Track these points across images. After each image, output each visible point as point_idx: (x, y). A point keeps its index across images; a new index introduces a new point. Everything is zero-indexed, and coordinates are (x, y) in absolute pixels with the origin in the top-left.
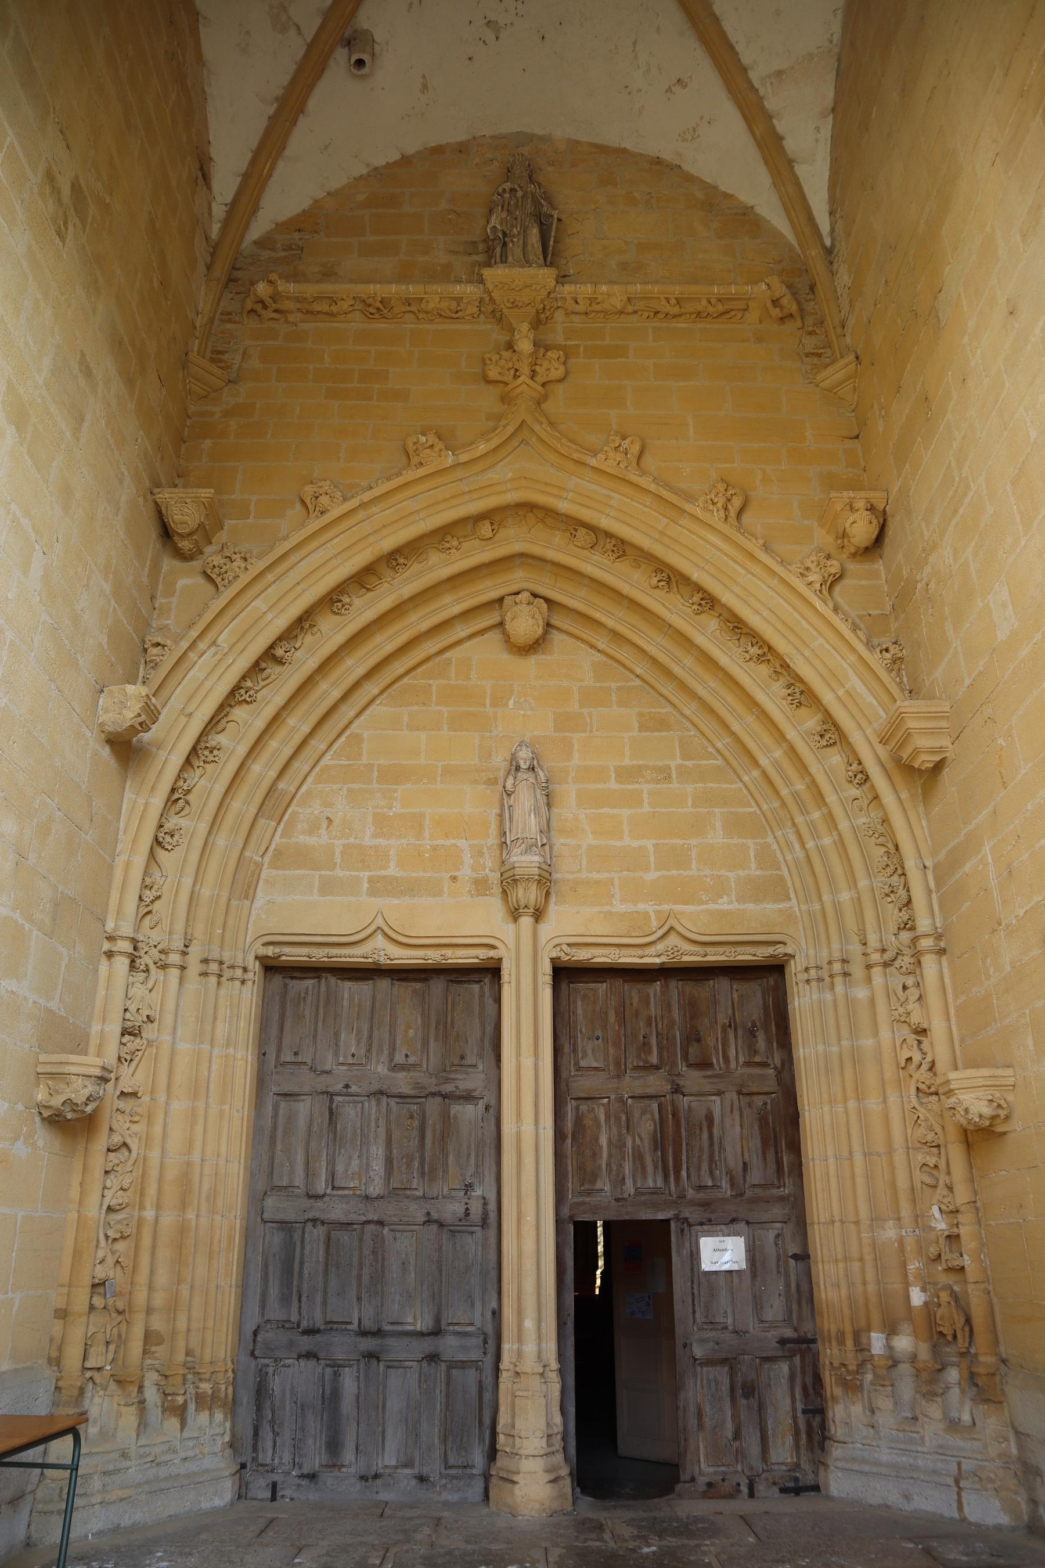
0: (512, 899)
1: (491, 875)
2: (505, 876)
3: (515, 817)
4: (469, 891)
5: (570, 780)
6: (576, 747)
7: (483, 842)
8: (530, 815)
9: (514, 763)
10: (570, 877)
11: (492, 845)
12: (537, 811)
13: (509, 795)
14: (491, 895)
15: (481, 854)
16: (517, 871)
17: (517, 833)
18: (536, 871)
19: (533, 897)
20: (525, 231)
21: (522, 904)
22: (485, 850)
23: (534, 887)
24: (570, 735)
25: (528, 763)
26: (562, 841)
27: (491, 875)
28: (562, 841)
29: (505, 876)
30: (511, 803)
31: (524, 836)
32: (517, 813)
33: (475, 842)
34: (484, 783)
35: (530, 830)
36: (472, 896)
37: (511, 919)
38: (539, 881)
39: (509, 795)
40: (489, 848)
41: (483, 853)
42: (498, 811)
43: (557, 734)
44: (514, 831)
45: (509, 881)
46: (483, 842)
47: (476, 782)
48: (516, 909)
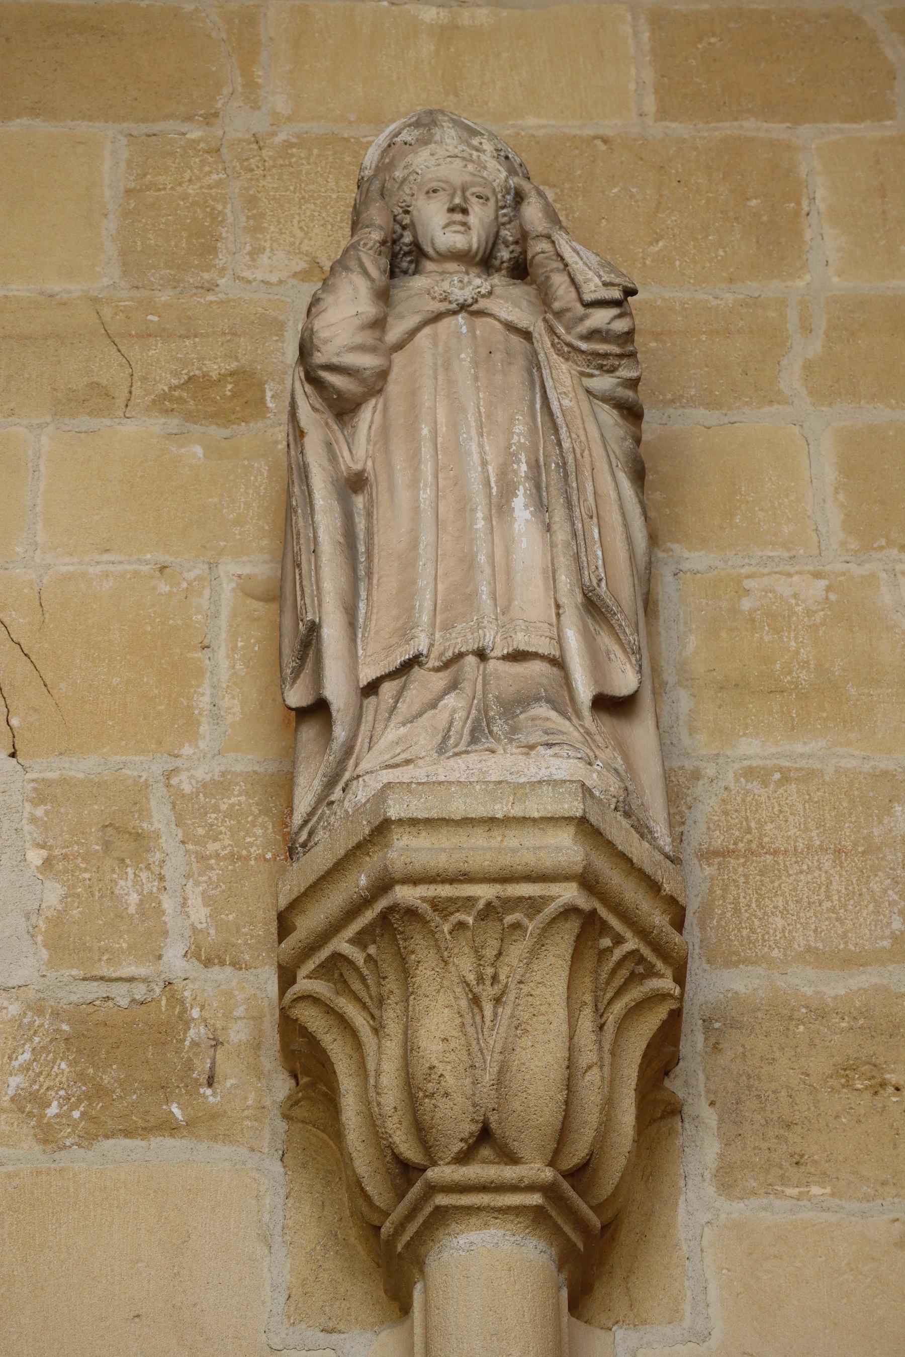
0: (369, 1091)
1: (206, 987)
2: (308, 924)
3: (390, 538)
4: (29, 1103)
5: (791, 378)
6: (821, 193)
7: (146, 766)
8: (501, 507)
9: (376, 214)
10: (836, 986)
11: (220, 786)
12: (554, 482)
13: (343, 409)
14: (203, 1125)
15: (126, 840)
16: (408, 850)
17: (405, 633)
18: (563, 848)
19: (539, 1061)
20: (512, 421)
21: (454, 1119)
22: (159, 817)
23: (544, 984)
24: (778, 130)
25: (480, 216)
26: (752, 748)
27: (206, 987)
28: (752, 748)
29: (308, 924)
30: (359, 452)
31: (462, 639)
32: (404, 512)
33: (81, 767)
34: (164, 403)
35: (504, 608)
36: (47, 1136)
37: (360, 1293)
38: (590, 925)
39: (343, 409)
40: (182, 807)
41: (141, 841)
42: (258, 566)
43: (679, 129)
44: (380, 618)
45: (351, 933)
46: (146, 766)
47: (97, 399)
48: (405, 1172)
